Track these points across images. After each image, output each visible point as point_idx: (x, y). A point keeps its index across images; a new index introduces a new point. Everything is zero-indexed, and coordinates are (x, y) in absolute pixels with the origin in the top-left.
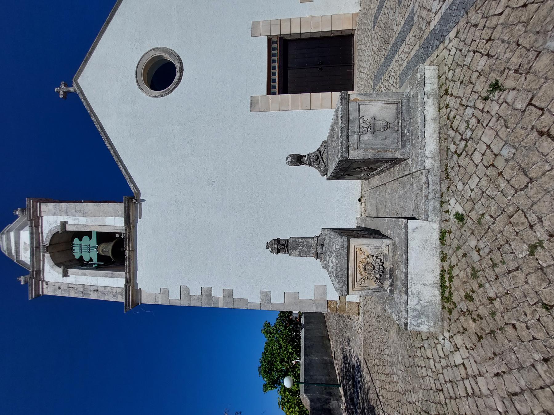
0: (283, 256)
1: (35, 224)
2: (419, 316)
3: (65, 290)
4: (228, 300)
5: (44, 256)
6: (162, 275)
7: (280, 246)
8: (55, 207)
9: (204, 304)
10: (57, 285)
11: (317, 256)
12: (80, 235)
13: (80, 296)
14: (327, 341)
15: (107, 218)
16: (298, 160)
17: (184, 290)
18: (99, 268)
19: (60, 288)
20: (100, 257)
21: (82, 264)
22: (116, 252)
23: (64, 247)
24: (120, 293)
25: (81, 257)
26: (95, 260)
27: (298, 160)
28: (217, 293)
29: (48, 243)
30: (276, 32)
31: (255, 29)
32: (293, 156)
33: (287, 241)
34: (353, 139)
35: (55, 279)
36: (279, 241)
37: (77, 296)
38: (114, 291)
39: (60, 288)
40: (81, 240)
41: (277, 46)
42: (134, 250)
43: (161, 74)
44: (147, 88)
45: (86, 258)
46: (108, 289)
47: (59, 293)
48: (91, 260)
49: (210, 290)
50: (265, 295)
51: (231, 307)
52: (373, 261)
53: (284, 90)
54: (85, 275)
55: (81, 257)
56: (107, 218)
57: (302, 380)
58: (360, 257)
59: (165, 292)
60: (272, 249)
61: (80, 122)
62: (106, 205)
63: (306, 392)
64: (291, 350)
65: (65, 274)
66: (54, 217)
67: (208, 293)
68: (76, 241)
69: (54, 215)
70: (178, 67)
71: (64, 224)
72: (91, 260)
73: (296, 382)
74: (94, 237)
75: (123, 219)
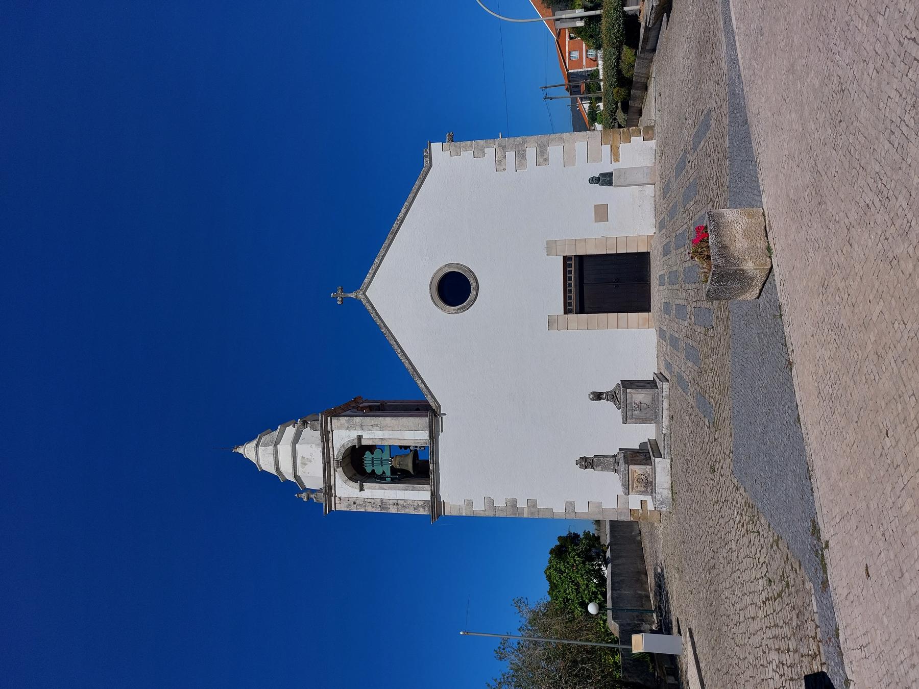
0: (589, 471)
1: (326, 438)
2: (661, 504)
3: (360, 505)
4: (533, 510)
5: (335, 471)
6: (462, 488)
7: (587, 463)
8: (348, 422)
9: (509, 514)
10: (352, 501)
11: (615, 471)
12: (371, 448)
13: (379, 510)
14: (643, 576)
15: (407, 432)
16: (598, 396)
17: (490, 502)
18: (394, 481)
19: (355, 503)
20: (393, 470)
22: (417, 467)
23: (357, 462)
24: (423, 507)
25: (373, 471)
26: (388, 473)
27: (598, 396)
28: (522, 504)
29: (341, 457)
31: (550, 248)
32: (593, 393)
33: (592, 459)
34: (629, 413)
35: (348, 493)
36: (585, 459)
37: (374, 510)
38: (416, 504)
39: (355, 503)
40: (372, 453)
41: (572, 263)
42: (437, 463)
43: (454, 289)
44: (441, 304)
45: (379, 471)
46: (409, 502)
47: (353, 508)
48: (384, 473)
49: (515, 500)
50: (570, 505)
51: (536, 516)
52: (642, 477)
53: (581, 310)
54: (383, 489)
55: (373, 471)
56: (407, 432)
57: (609, 604)
58: (635, 475)
59: (470, 503)
61: (369, 339)
62: (405, 419)
63: (614, 619)
64: (594, 589)
65: (362, 489)
66: (345, 434)
67: (513, 504)
68: (368, 454)
69: (347, 429)
70: (473, 285)
71: (360, 438)
72: (384, 473)
73: (602, 607)
74: (387, 452)
75: (428, 433)
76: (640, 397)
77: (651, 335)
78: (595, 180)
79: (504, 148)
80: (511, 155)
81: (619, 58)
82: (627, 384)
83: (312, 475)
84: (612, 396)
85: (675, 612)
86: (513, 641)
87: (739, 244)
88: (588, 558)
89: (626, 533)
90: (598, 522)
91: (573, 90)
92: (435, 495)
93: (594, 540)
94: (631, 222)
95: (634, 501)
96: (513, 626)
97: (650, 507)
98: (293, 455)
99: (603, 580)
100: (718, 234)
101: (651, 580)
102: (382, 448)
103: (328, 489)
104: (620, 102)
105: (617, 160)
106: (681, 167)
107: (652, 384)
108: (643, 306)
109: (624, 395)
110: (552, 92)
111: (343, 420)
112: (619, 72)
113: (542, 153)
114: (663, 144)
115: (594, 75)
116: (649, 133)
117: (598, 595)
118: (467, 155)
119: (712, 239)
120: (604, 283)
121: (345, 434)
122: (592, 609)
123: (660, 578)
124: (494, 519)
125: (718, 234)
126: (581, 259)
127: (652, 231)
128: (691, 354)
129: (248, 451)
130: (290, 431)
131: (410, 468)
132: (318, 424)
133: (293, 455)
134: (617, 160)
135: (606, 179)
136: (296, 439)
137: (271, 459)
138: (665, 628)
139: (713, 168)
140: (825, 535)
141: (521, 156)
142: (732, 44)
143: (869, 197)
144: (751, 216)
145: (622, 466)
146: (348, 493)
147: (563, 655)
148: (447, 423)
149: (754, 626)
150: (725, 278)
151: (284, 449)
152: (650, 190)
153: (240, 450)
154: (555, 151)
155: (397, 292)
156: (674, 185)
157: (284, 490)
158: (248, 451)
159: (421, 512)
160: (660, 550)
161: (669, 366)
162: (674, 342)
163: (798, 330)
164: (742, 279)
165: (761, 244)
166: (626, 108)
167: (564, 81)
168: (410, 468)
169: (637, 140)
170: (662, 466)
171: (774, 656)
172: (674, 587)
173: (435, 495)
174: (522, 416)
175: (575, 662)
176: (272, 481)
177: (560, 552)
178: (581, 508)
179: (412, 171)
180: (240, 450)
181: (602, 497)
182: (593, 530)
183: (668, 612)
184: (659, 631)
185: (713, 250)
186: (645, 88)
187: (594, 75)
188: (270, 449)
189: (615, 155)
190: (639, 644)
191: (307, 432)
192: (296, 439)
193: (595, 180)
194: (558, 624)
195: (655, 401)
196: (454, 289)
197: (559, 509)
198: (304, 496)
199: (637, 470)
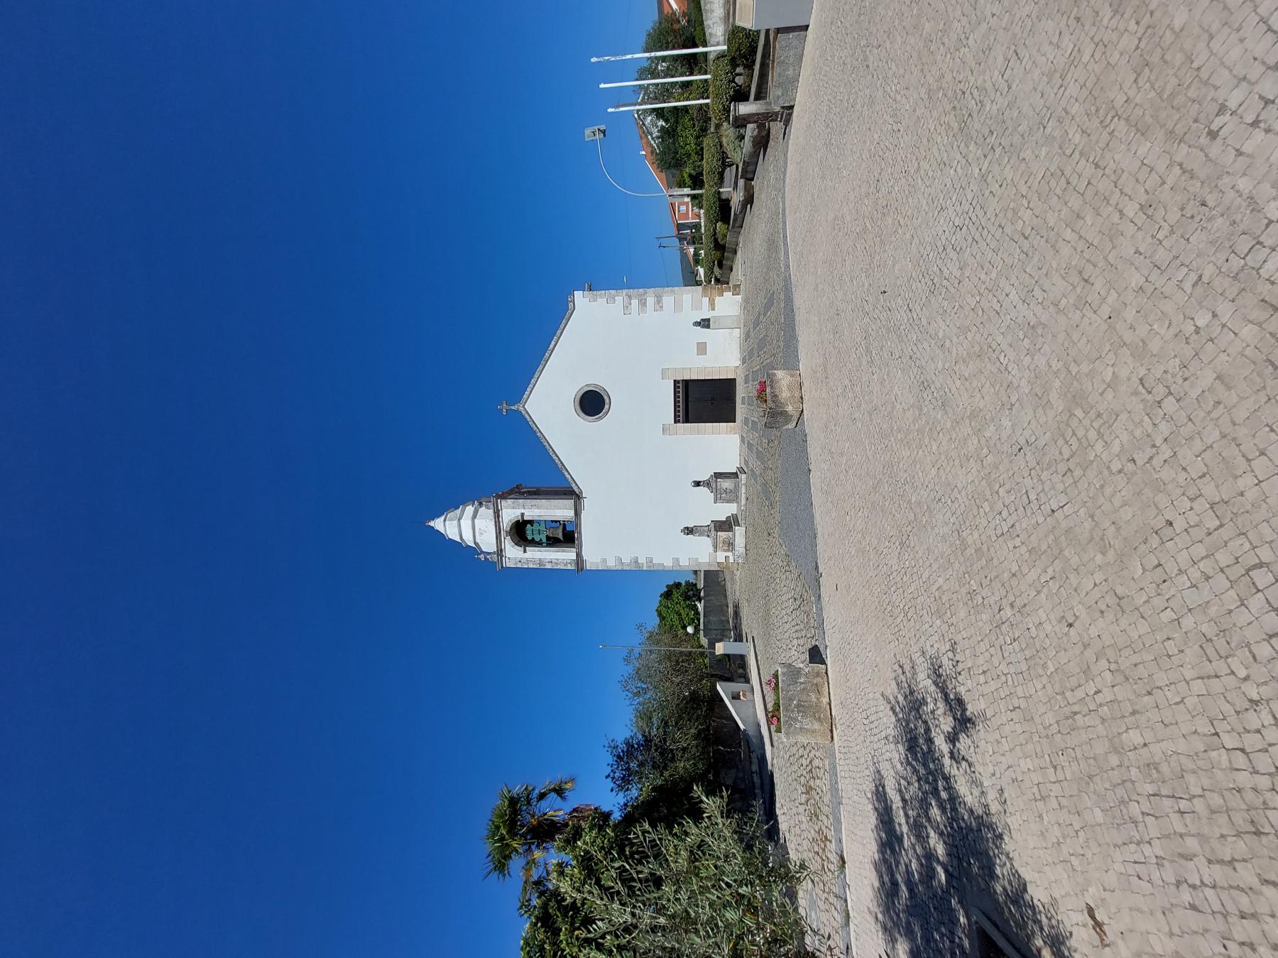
1: (497, 515)
6: (599, 549)
7: (689, 531)
12: (531, 522)
15: (559, 510)
16: (697, 484)
18: (549, 545)
20: (548, 538)
21: (533, 543)
22: (566, 536)
23: (520, 532)
26: (544, 540)
27: (697, 484)
28: (642, 560)
30: (679, 378)
31: (664, 373)
42: (580, 533)
45: (537, 539)
47: (519, 565)
49: (677, 560)
53: (687, 421)
56: (559, 510)
57: (702, 627)
59: (605, 560)
60: (734, 790)
61: (529, 439)
66: (511, 511)
71: (523, 515)
73: (697, 629)
76: (726, 484)
77: (736, 439)
78: (697, 324)
79: (630, 297)
80: (635, 302)
81: (715, 229)
82: (718, 475)
83: (488, 542)
84: (707, 484)
85: (745, 629)
86: (637, 651)
87: (784, 394)
88: (687, 598)
89: (714, 579)
90: (695, 572)
91: (681, 239)
92: (579, 555)
93: (692, 586)
94: (722, 357)
95: (721, 557)
96: (636, 641)
97: (731, 560)
98: (473, 526)
99: (697, 613)
100: (772, 387)
101: (731, 610)
102: (539, 522)
103: (500, 552)
104: (713, 257)
105: (713, 309)
106: (756, 324)
107: (735, 475)
108: (729, 417)
109: (716, 482)
110: (665, 242)
111: (510, 501)
112: (716, 240)
113: (659, 300)
114: (746, 300)
115: (697, 226)
116: (736, 290)
117: (695, 621)
118: (601, 301)
119: (768, 390)
120: (703, 401)
121: (511, 511)
122: (690, 630)
123: (736, 607)
124: (622, 571)
125: (772, 387)
126: (687, 384)
127: (738, 363)
128: (760, 456)
129: (438, 524)
130: (470, 509)
131: (560, 536)
132: (491, 505)
133: (473, 526)
134: (713, 309)
135: (705, 323)
136: (474, 516)
137: (456, 530)
138: (739, 638)
139: (772, 333)
140: (821, 570)
141: (643, 303)
142: (786, 253)
143: (847, 382)
144: (792, 376)
145: (713, 532)
146: (514, 554)
147: (669, 659)
148: (587, 503)
149: (787, 626)
150: (775, 416)
151: (466, 523)
152: (737, 332)
153: (432, 524)
154: (668, 300)
155: (548, 404)
156: (752, 334)
157: (465, 554)
158: (438, 524)
159: (569, 567)
160: (737, 590)
161: (746, 463)
162: (750, 446)
163: (814, 451)
164: (786, 416)
165: (797, 394)
166: (720, 265)
167: (675, 232)
168: (560, 536)
169: (728, 294)
170: (739, 531)
171: (795, 642)
172: (745, 612)
173: (579, 555)
174: (645, 501)
175: (677, 662)
176: (458, 548)
177: (668, 595)
178: (684, 563)
179: (558, 314)
180: (432, 524)
181: (699, 554)
182: (692, 580)
183: (741, 630)
184: (735, 641)
185: (769, 398)
186: (735, 252)
187: (697, 226)
188: (455, 522)
189: (712, 306)
190: (720, 648)
191: (482, 510)
192: (474, 516)
193: (697, 324)
194: (666, 638)
195: (737, 487)
196: (592, 403)
197: (668, 564)
198: (482, 557)
199: (722, 535)
